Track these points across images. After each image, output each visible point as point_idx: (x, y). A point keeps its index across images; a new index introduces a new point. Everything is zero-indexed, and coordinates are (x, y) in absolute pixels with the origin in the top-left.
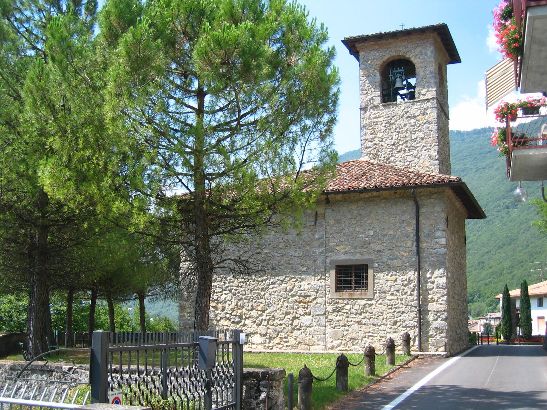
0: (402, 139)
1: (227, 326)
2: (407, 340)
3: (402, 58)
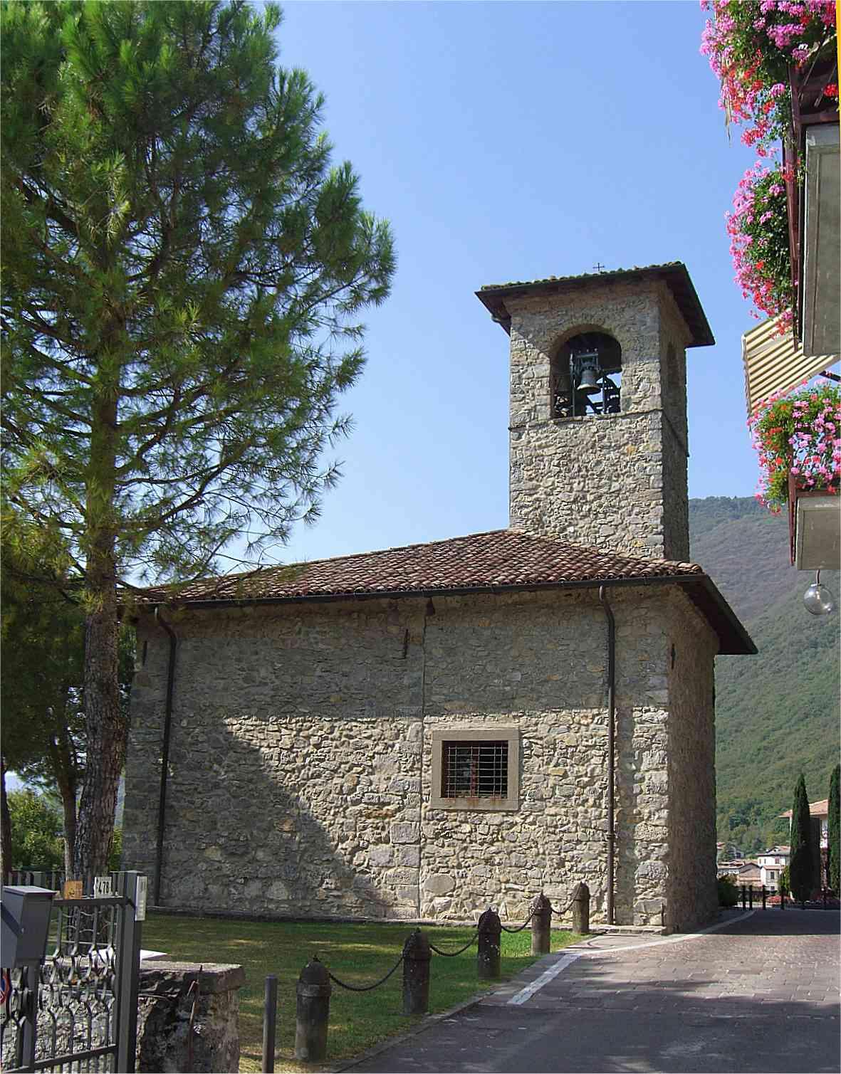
0: (592, 491)
1: (219, 862)
2: (582, 896)
3: (597, 330)
